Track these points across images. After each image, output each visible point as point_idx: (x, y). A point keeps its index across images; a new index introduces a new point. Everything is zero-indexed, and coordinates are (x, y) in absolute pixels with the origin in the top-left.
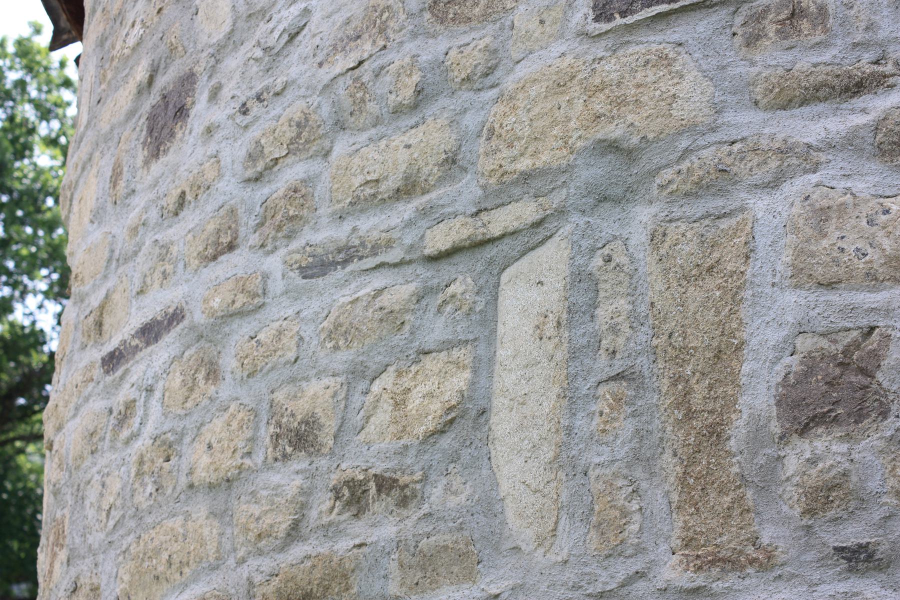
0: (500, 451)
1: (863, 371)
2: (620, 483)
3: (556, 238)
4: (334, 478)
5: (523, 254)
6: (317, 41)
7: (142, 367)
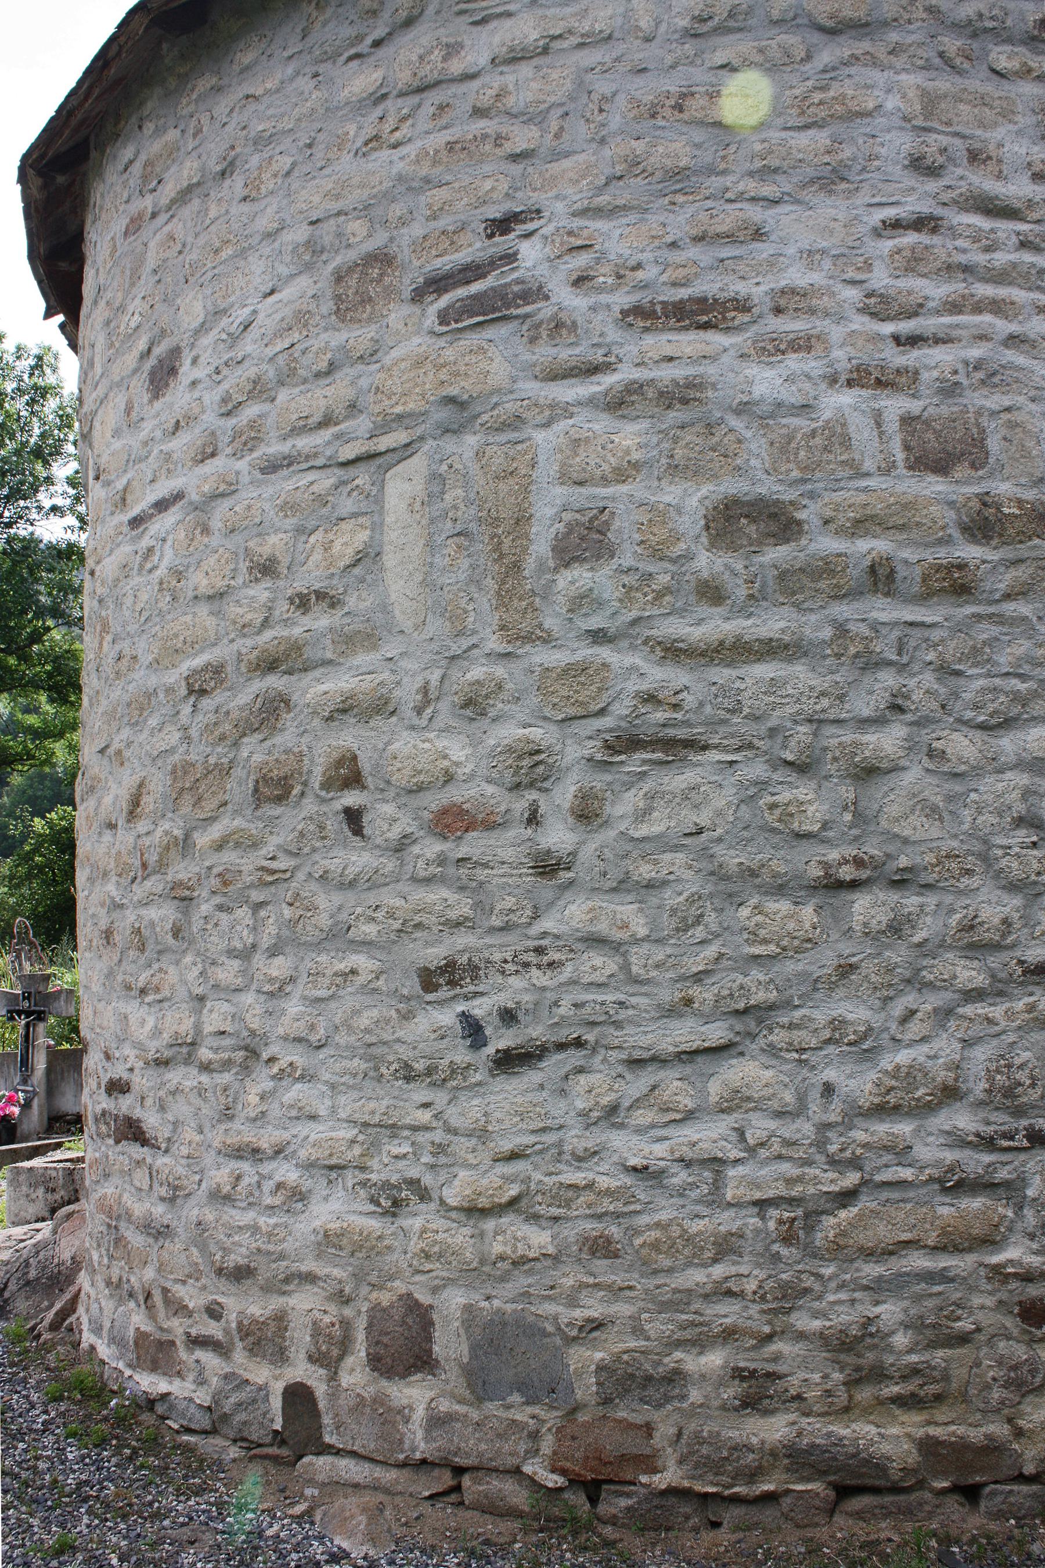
0: (389, 577)
1: (599, 532)
2: (462, 594)
3: (419, 453)
4: (290, 592)
5: (399, 462)
6: (263, 330)
7: (157, 526)
